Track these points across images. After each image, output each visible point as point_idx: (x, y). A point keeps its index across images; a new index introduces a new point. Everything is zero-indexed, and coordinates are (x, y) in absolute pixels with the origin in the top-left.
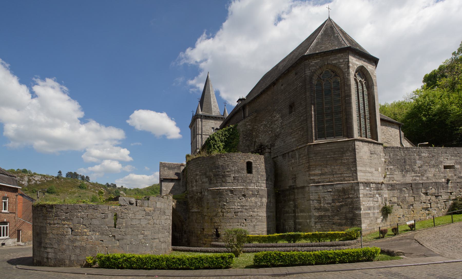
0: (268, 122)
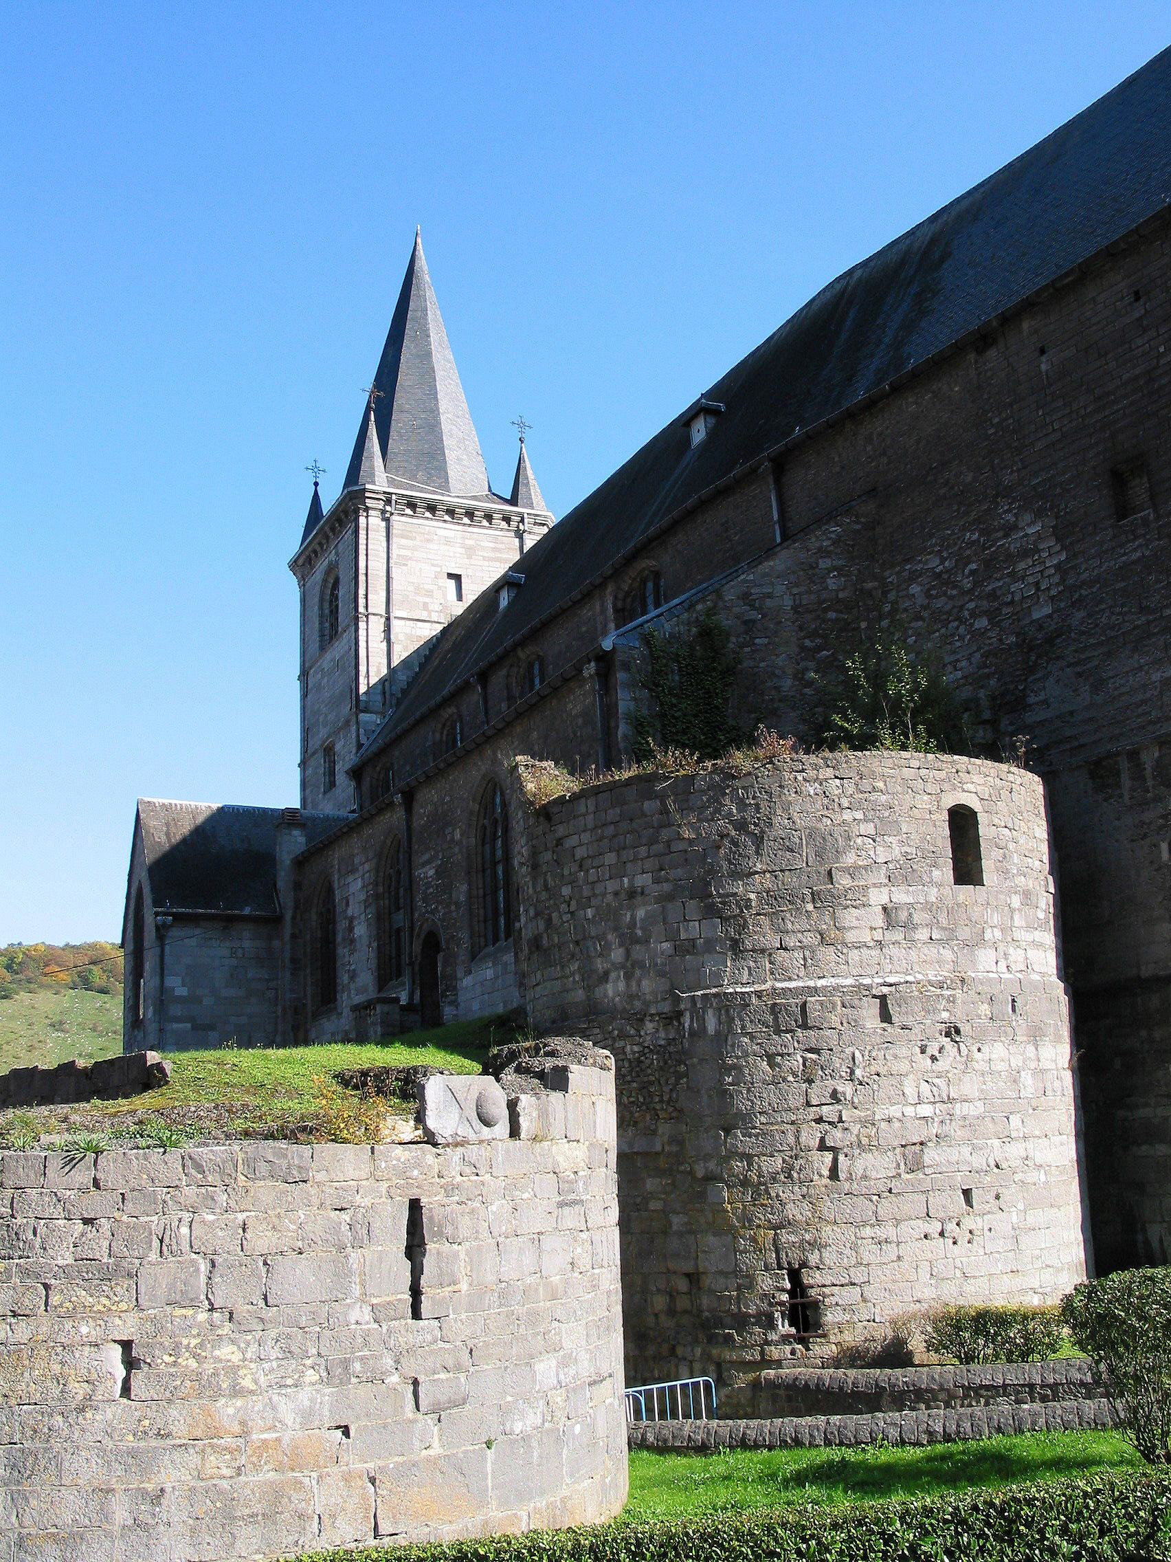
0: (963, 562)
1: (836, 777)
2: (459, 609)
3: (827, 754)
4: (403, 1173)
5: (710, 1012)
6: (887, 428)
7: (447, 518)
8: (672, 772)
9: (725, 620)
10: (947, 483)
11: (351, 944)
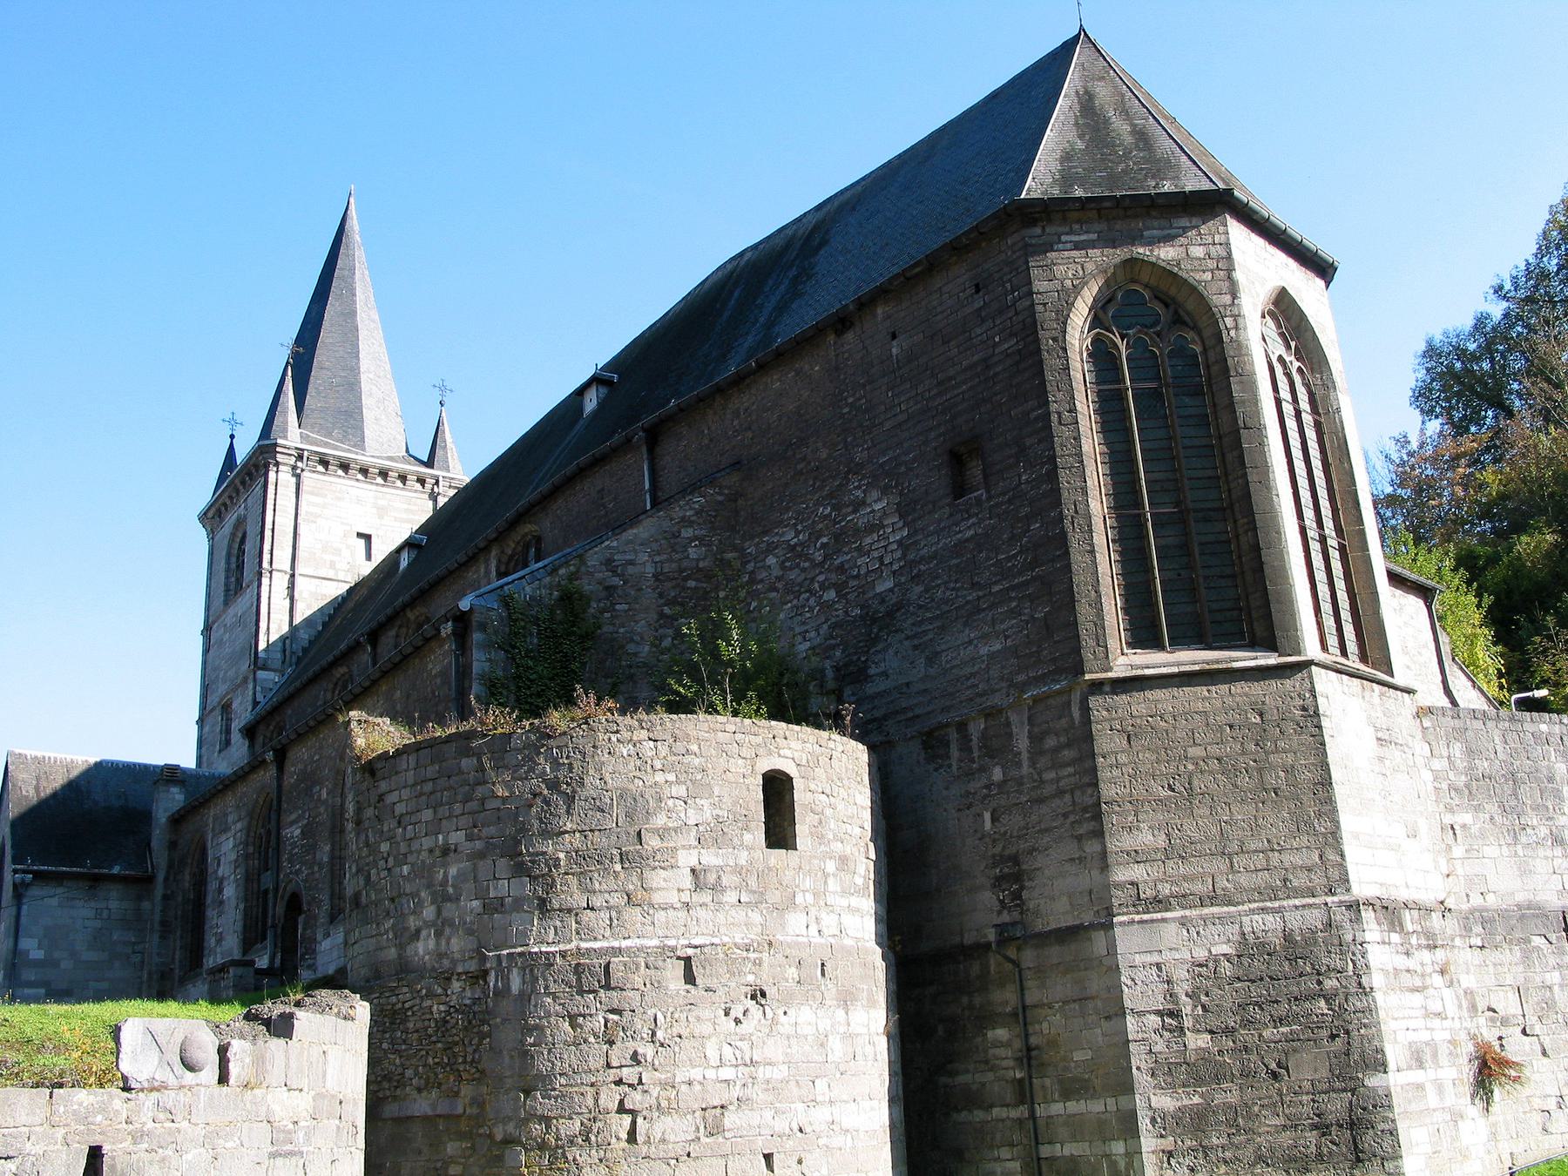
1: (650, 739)
2: (366, 569)
3: (644, 716)
4: (85, 1120)
5: (515, 971)
6: (753, 404)
7: (360, 476)
8: (490, 730)
9: (587, 586)
10: (804, 459)
11: (219, 906)
